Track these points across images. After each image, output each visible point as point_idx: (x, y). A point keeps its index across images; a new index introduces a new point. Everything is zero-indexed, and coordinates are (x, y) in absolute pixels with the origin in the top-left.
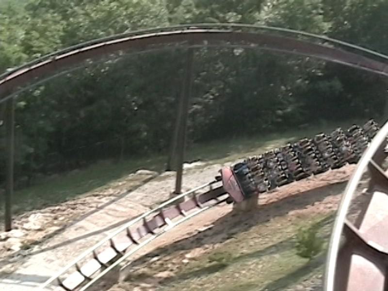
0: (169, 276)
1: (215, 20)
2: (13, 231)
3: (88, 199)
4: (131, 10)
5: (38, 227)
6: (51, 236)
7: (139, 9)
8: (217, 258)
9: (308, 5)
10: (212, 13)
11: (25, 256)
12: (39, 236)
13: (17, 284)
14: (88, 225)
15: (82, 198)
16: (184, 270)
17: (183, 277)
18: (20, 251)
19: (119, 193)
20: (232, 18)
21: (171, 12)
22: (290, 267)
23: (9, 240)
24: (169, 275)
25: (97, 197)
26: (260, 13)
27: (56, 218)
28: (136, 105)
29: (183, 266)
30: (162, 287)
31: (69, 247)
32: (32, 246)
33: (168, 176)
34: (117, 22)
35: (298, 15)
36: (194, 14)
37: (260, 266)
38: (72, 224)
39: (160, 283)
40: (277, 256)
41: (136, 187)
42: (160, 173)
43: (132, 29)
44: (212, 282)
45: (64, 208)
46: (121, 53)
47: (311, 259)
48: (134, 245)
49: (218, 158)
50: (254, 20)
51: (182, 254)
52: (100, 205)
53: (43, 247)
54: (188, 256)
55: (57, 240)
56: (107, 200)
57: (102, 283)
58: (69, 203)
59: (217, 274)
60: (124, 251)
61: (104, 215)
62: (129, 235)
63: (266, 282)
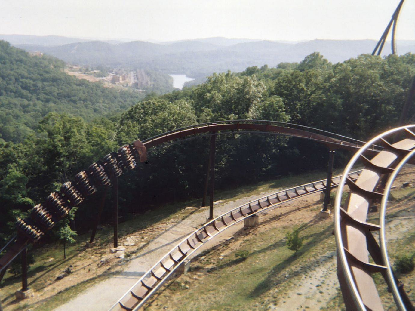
0: (213, 268)
1: (223, 119)
2: (119, 247)
3: (160, 226)
4: (176, 116)
5: (134, 244)
6: (142, 248)
7: (180, 116)
8: (240, 254)
9: (276, 107)
10: (221, 116)
11: (128, 261)
12: (135, 249)
13: (125, 278)
14: (162, 240)
15: (156, 226)
16: (221, 263)
17: (221, 267)
18: (124, 258)
19: (177, 221)
20: (233, 117)
21: (198, 117)
22: (285, 256)
23: (118, 252)
24: (212, 266)
25: (165, 224)
26: (248, 113)
27: (143, 238)
28: (181, 170)
29: (220, 261)
30: (210, 274)
31: (152, 254)
32: (130, 255)
33: (204, 210)
34: (168, 124)
35: (271, 113)
36: (211, 117)
37: (266, 258)
38: (153, 241)
39: (208, 272)
40: (275, 251)
41: (187, 217)
42: (199, 208)
43: (177, 127)
44: (239, 269)
45: (147, 232)
46: (171, 141)
47: (297, 250)
48: (192, 249)
49: (231, 197)
50: (246, 117)
51: (219, 254)
52: (167, 229)
53: (138, 255)
54: (222, 255)
55: (145, 250)
56: (170, 225)
57: (175, 274)
58: (148, 228)
59: (241, 264)
60: (186, 253)
61: (170, 234)
62: (188, 243)
63: (272, 267)
